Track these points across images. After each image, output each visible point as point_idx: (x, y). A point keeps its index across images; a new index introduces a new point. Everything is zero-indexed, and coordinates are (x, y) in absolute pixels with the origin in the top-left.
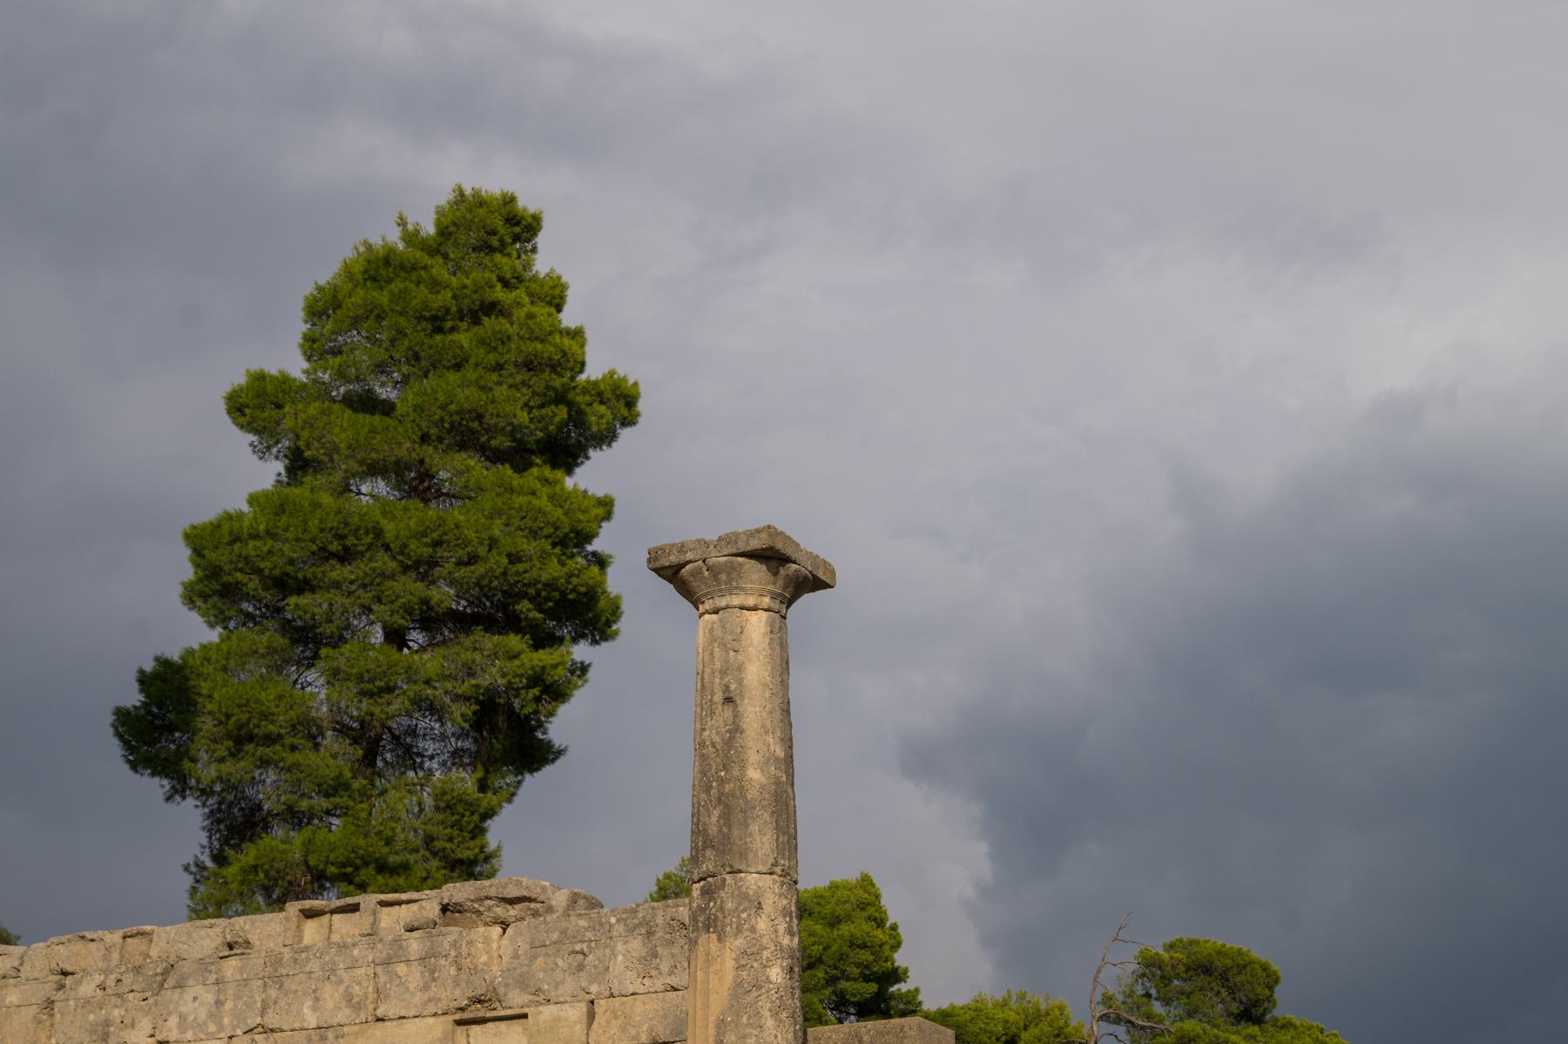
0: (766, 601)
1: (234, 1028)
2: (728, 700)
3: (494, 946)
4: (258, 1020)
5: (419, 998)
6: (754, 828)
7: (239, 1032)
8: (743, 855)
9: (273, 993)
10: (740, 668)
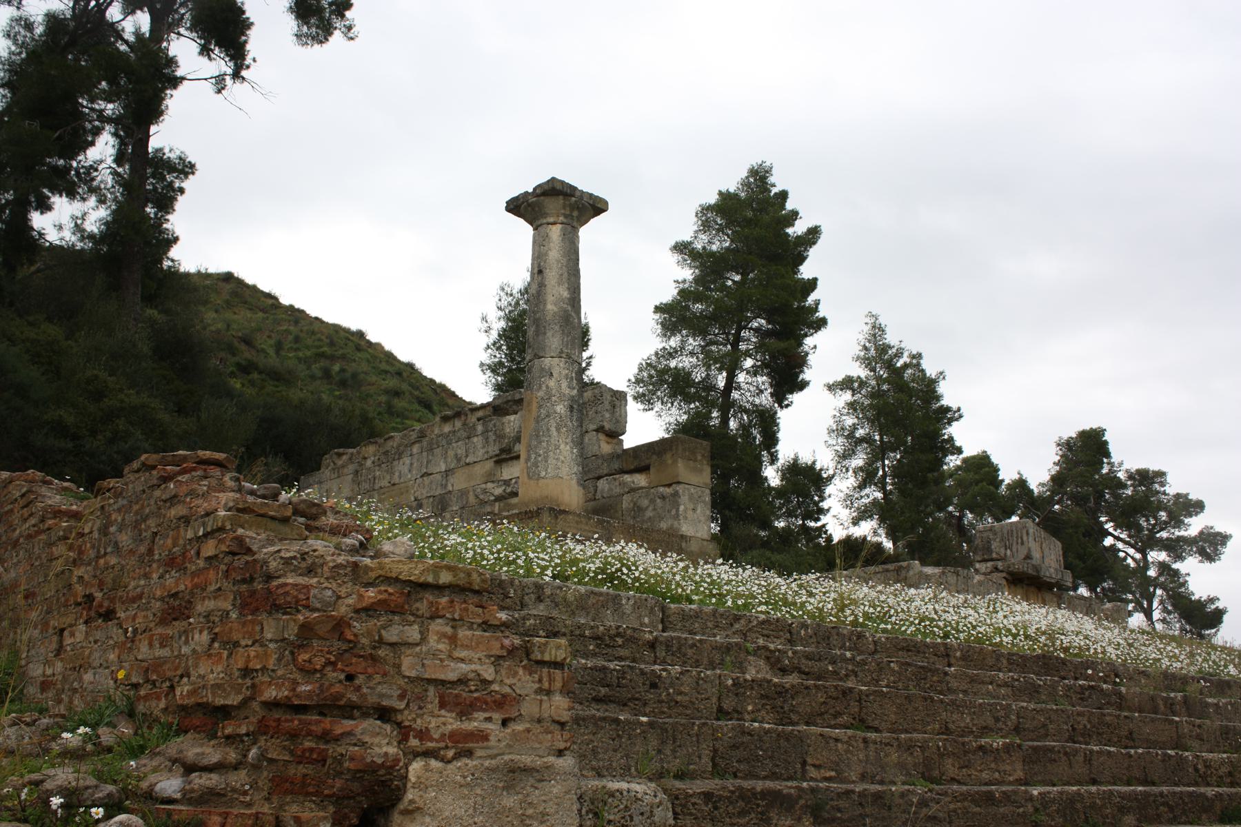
0: (561, 219)
2: (540, 272)
6: (549, 334)
10: (546, 254)
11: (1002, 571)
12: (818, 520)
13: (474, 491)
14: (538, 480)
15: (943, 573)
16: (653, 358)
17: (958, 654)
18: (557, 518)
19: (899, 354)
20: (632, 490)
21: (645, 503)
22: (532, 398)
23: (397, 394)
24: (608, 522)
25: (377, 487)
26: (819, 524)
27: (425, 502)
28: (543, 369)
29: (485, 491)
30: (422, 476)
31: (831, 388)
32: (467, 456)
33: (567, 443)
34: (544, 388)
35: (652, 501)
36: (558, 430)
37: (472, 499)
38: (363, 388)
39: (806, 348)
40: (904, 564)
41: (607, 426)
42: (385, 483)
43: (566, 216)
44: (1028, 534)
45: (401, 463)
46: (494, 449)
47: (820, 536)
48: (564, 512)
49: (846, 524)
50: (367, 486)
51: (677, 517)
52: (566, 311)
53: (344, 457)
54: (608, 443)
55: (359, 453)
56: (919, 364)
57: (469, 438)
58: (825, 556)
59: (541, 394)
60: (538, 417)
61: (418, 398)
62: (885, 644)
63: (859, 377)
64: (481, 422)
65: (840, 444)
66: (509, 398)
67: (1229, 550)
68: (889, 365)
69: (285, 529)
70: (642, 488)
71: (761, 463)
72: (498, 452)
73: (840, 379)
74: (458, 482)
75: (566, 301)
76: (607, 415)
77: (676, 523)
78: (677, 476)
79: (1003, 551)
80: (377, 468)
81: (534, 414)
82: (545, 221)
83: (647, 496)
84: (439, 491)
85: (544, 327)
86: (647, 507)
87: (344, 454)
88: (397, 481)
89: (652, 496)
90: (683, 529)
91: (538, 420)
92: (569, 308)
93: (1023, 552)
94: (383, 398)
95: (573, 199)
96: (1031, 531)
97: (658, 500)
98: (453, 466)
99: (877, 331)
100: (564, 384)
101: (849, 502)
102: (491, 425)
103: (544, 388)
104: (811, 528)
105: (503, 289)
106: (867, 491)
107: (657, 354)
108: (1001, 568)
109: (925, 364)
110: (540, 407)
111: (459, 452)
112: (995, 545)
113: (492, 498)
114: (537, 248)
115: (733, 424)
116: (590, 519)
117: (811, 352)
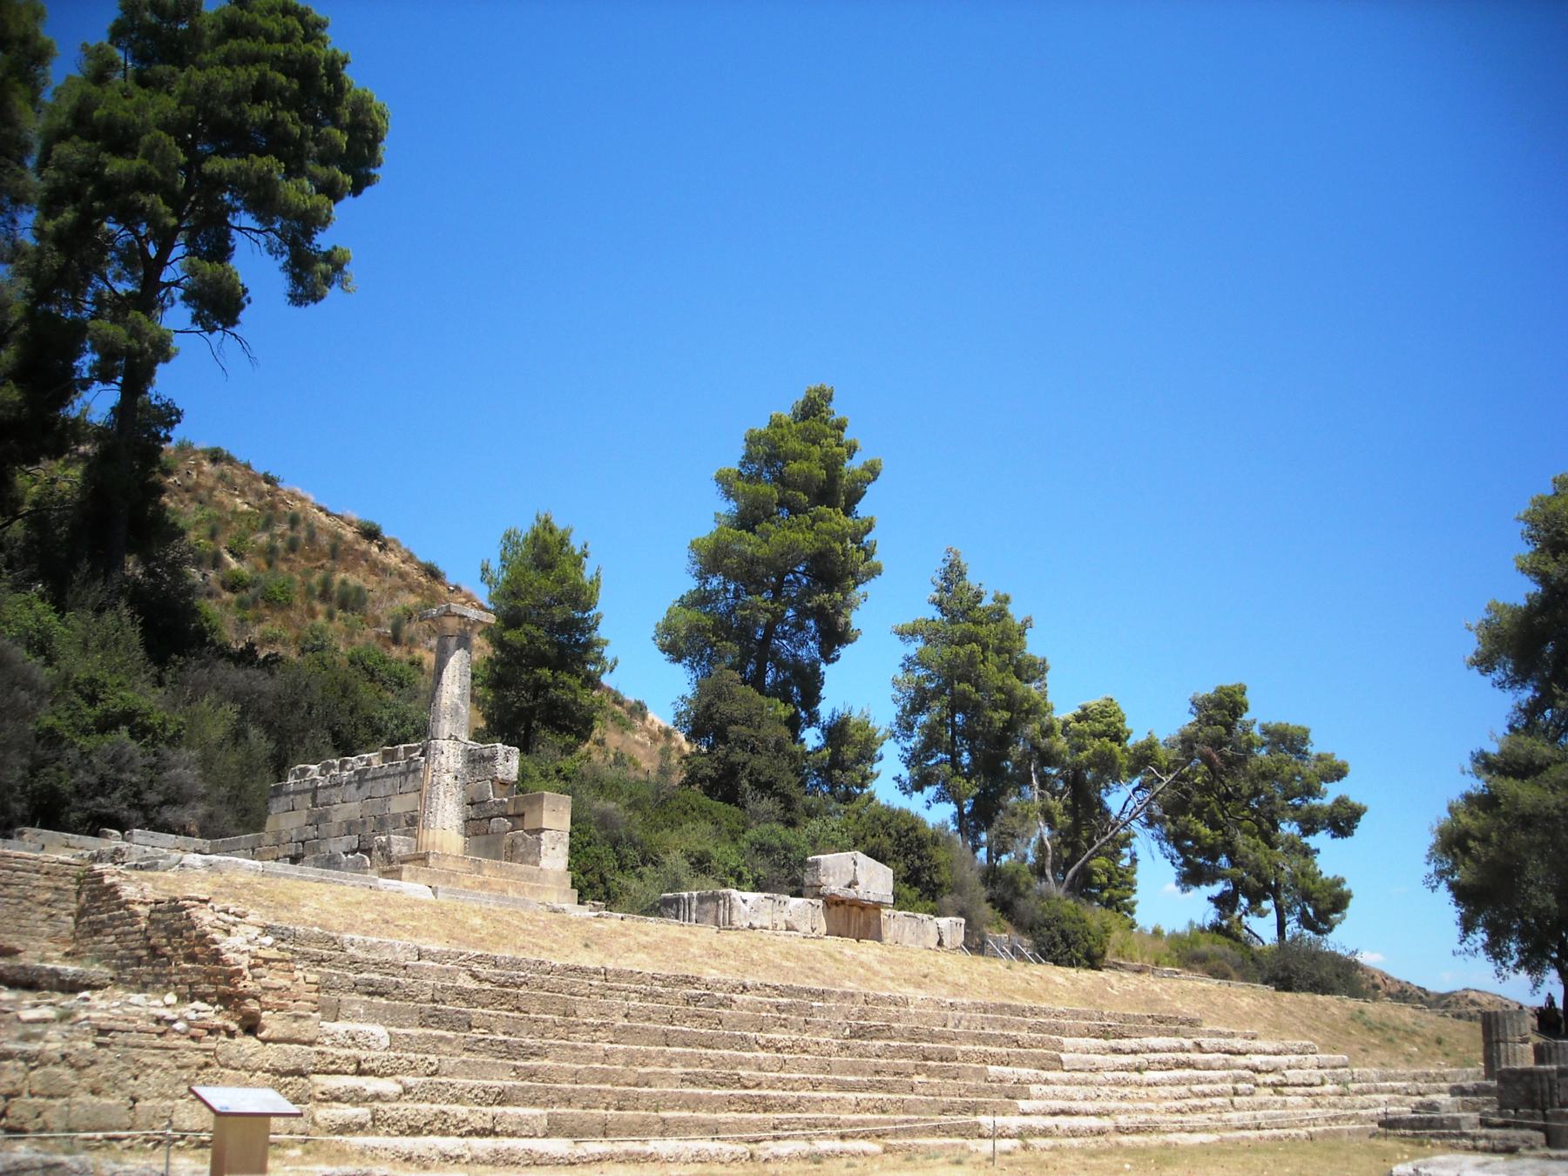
6: (443, 721)
67: (1363, 826)
99: (953, 574)
100: (452, 759)
109: (1011, 609)
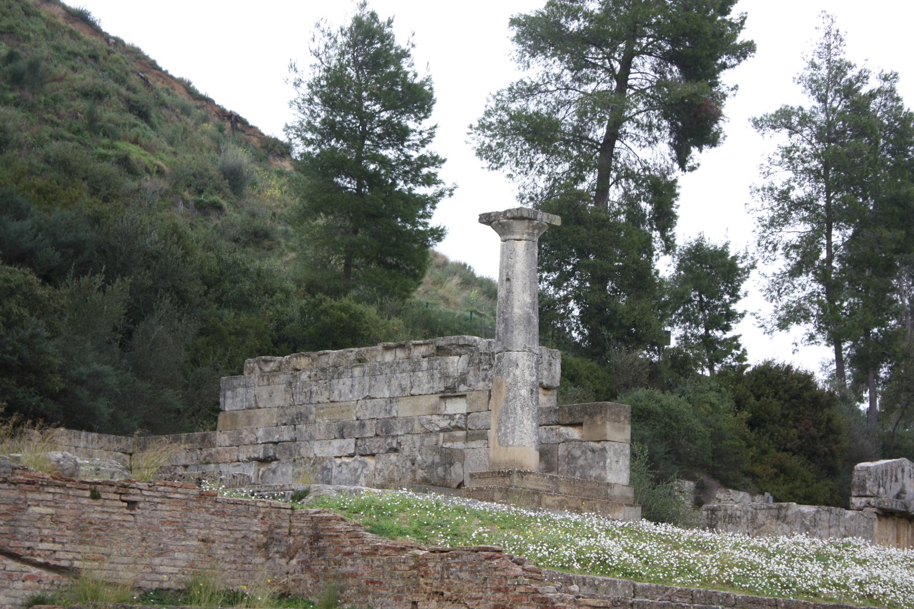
0: (525, 236)
1: (359, 396)
2: (508, 280)
3: (456, 365)
4: (368, 394)
5: (426, 386)
6: (516, 333)
7: (360, 398)
8: (511, 345)
9: (373, 382)
10: (513, 266)
11: (874, 507)
12: (727, 328)
13: (419, 420)
14: (507, 446)
15: (818, 511)
16: (506, 93)
17: (783, 605)
18: (522, 477)
19: (862, 77)
20: (566, 441)
21: (578, 453)
22: (502, 383)
23: (98, 96)
24: (556, 478)
25: (314, 400)
26: (729, 335)
27: (368, 423)
28: (510, 361)
29: (430, 422)
30: (364, 398)
31: (757, 124)
32: (412, 387)
33: (528, 419)
34: (512, 376)
35: (584, 452)
36: (522, 409)
37: (417, 427)
38: (47, 87)
39: (724, 89)
40: (785, 504)
41: (545, 382)
42: (323, 398)
43: (529, 234)
44: (903, 471)
45: (341, 381)
46: (440, 386)
47: (728, 352)
48: (526, 473)
49: (769, 326)
50: (302, 398)
51: (604, 468)
52: (528, 314)
53: (272, 364)
54: (544, 395)
55: (288, 362)
56: (892, 90)
57: (413, 371)
58: (734, 391)
59: (509, 380)
60: (507, 398)
61: (128, 101)
62: (741, 600)
63: (801, 109)
64: (426, 359)
65: (767, 209)
66: (454, 342)
68: (849, 91)
69: (541, 583)
70: (575, 440)
71: (650, 252)
72: (443, 389)
73: (772, 111)
74: (402, 410)
75: (529, 305)
76: (545, 373)
77: (603, 473)
78: (605, 435)
79: (875, 489)
80: (314, 383)
81: (504, 395)
82: (512, 237)
83: (580, 447)
84: (382, 415)
85: (512, 327)
86: (580, 457)
87: (271, 361)
88: (337, 399)
89: (583, 448)
90: (609, 478)
91: (507, 400)
92: (531, 311)
93: (896, 489)
94: (81, 105)
95: (536, 222)
96: (907, 469)
97: (589, 453)
98: (397, 394)
100: (527, 373)
101: (775, 293)
102: (436, 364)
103: (512, 376)
104: (716, 341)
105: (318, 25)
106: (803, 279)
107: (510, 89)
108: (873, 504)
110: (509, 390)
111: (403, 382)
112: (869, 484)
113: (438, 429)
114: (505, 259)
115: (615, 194)
116: (544, 476)
117: (730, 94)
